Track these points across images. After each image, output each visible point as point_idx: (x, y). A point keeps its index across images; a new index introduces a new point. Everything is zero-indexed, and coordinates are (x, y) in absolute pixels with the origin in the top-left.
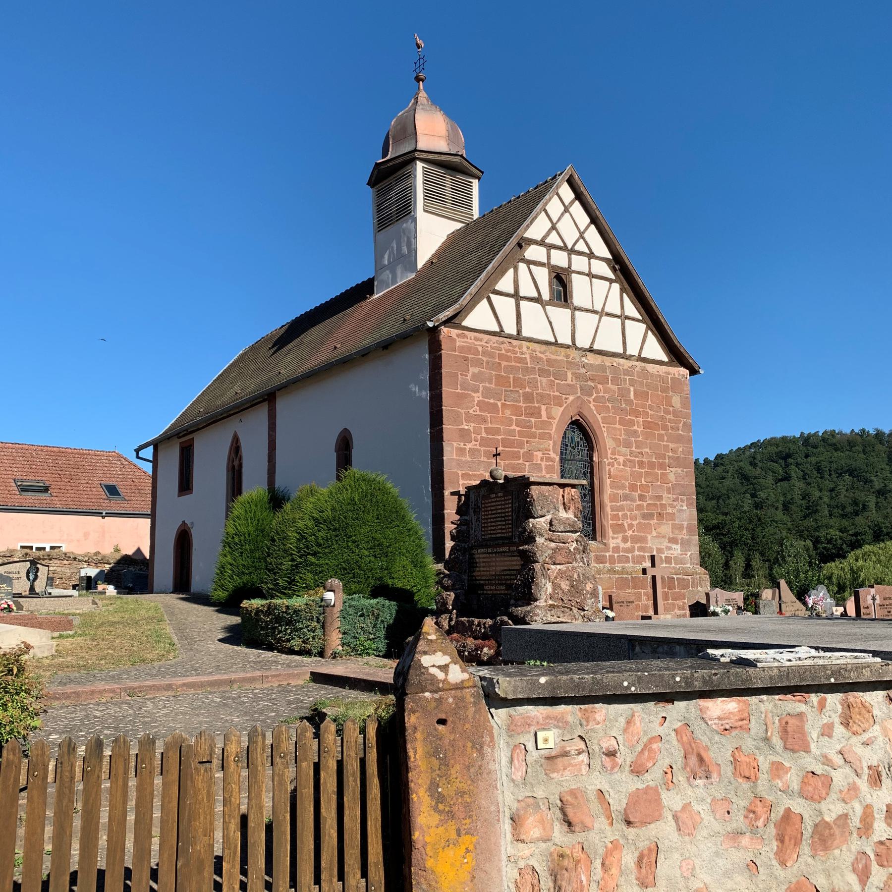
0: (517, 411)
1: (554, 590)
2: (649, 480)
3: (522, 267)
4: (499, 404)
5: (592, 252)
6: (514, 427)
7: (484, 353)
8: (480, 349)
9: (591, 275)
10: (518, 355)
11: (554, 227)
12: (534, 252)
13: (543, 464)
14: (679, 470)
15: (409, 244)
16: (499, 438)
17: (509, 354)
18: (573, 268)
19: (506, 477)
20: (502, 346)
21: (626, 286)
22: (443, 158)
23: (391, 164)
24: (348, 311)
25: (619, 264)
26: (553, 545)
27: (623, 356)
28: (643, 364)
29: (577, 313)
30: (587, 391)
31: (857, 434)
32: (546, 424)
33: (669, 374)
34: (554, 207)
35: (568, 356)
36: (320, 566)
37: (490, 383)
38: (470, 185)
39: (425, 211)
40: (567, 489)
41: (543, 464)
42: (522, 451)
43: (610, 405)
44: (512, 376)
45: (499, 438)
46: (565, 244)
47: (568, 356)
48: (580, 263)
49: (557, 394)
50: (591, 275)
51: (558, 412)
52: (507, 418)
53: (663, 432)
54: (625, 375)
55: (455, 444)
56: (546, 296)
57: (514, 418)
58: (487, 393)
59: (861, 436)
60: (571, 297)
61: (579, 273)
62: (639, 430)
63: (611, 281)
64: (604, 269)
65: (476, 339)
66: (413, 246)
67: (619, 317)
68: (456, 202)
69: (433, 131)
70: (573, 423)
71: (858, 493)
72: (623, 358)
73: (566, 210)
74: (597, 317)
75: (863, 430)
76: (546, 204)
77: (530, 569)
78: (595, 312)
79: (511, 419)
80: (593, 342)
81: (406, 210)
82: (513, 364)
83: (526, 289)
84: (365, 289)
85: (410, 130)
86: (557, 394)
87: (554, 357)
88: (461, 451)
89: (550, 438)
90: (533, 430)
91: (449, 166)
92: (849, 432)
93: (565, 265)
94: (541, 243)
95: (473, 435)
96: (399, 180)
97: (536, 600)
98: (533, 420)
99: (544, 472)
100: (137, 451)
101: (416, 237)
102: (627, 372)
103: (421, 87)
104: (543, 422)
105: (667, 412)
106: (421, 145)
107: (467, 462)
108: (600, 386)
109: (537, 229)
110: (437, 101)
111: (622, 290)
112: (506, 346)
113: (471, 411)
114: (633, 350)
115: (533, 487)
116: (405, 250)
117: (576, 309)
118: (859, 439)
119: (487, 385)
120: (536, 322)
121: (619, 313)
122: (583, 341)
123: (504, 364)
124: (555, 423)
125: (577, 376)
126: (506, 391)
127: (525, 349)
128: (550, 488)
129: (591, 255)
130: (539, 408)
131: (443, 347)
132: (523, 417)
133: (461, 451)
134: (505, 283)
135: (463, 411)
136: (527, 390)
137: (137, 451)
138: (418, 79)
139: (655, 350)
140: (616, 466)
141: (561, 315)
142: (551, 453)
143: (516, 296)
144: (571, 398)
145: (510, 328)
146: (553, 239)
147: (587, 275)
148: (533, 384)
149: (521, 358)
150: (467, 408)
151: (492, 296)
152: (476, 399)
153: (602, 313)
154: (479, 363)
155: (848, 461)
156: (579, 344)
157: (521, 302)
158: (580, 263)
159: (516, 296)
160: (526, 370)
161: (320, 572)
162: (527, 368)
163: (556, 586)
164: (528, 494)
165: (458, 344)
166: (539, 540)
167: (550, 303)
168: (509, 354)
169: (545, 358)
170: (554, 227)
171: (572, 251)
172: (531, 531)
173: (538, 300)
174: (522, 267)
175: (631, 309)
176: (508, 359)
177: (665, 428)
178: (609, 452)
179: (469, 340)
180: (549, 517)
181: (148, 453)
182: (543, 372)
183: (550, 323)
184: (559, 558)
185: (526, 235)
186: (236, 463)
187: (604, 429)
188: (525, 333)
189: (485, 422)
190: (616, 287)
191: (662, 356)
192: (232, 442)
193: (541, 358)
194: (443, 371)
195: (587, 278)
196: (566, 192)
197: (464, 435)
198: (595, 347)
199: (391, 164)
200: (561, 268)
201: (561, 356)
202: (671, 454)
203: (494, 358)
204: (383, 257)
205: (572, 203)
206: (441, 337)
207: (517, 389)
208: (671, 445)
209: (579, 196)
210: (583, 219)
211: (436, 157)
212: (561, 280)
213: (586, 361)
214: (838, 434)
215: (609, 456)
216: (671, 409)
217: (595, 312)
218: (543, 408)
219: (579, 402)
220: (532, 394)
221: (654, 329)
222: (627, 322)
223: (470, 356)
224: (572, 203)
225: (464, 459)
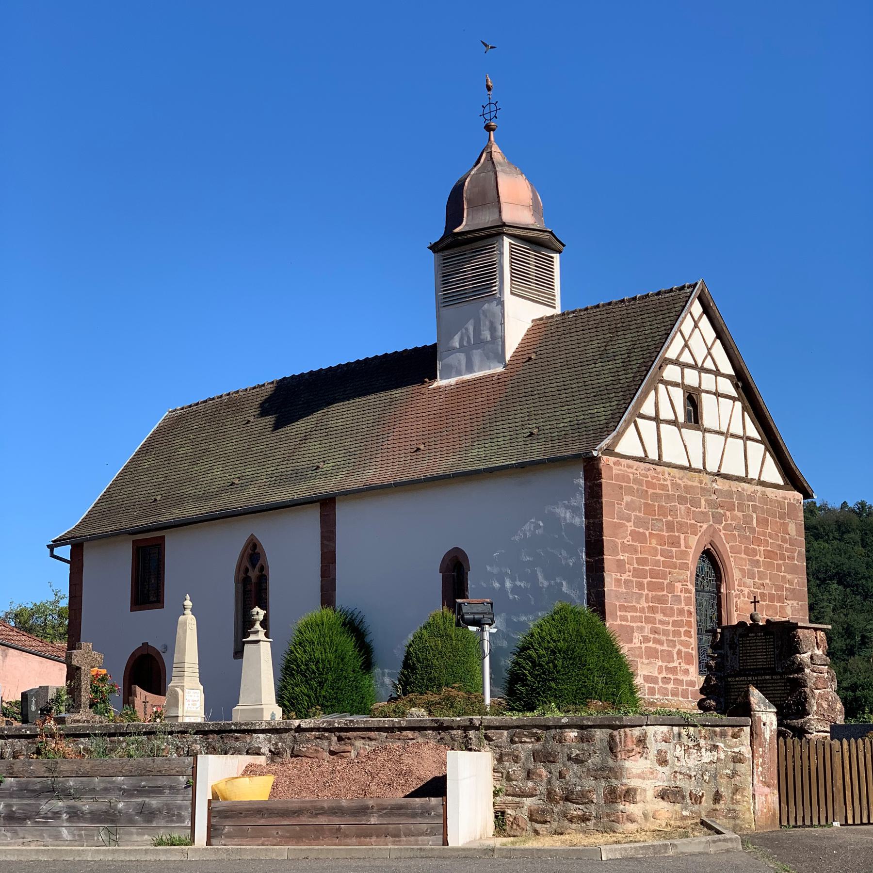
0: (661, 541)
1: (818, 708)
2: (770, 613)
3: (661, 387)
4: (647, 533)
5: (718, 370)
6: (659, 557)
7: (636, 481)
8: (631, 476)
9: (717, 394)
10: (662, 482)
11: (686, 345)
12: (671, 373)
13: (683, 595)
14: (795, 603)
15: (493, 329)
16: (648, 568)
17: (654, 481)
18: (703, 387)
19: (768, 621)
20: (648, 473)
21: (747, 404)
22: (532, 234)
23: (472, 235)
24: (397, 393)
25: (742, 381)
26: (815, 674)
27: (745, 480)
28: (764, 489)
29: (707, 434)
30: (718, 518)
31: (852, 510)
32: (684, 554)
33: (785, 498)
34: (687, 325)
35: (701, 482)
36: (561, 691)
37: (640, 512)
38: (551, 260)
39: (512, 293)
40: (819, 632)
41: (683, 595)
42: (666, 582)
43: (737, 534)
44: (656, 504)
45: (648, 568)
46: (696, 364)
47: (701, 482)
48: (708, 382)
49: (693, 522)
50: (717, 394)
51: (693, 540)
52: (654, 548)
53: (781, 562)
54: (748, 501)
55: (614, 576)
56: (681, 419)
57: (659, 547)
58: (639, 522)
59: (859, 515)
60: (702, 418)
61: (708, 392)
62: (761, 559)
63: (733, 399)
64: (727, 387)
65: (629, 467)
66: (499, 334)
67: (741, 438)
68: (539, 281)
69: (517, 200)
70: (704, 552)
71: (852, 616)
72: (745, 482)
73: (696, 326)
74: (723, 438)
75: (862, 505)
76: (681, 324)
77: (801, 693)
78: (721, 433)
79: (657, 550)
80: (720, 467)
81: (485, 288)
82: (658, 491)
83: (666, 413)
84: (417, 365)
85: (492, 194)
86: (693, 522)
87: (690, 483)
88: (618, 581)
89: (688, 568)
90: (674, 560)
91: (537, 242)
92: (838, 505)
93: (696, 384)
94: (676, 362)
95: (627, 566)
96: (477, 251)
97: (809, 714)
98: (674, 549)
99: (683, 604)
100: (51, 548)
101: (502, 324)
102: (750, 498)
103: (492, 139)
104: (682, 551)
105: (784, 540)
106: (509, 215)
107: (622, 593)
108: (728, 513)
109: (673, 350)
110: (521, 163)
111: (744, 409)
112: (652, 473)
113: (625, 541)
114: (753, 474)
115: (799, 630)
116: (486, 335)
117: (706, 431)
118: (855, 519)
119: (638, 514)
120: (678, 446)
121: (741, 434)
122: (712, 467)
123: (650, 491)
124: (691, 551)
125: (709, 503)
126: (653, 520)
127: (666, 476)
128: (809, 631)
129: (717, 373)
130: (679, 537)
131: (603, 476)
132: (666, 547)
133: (618, 581)
134: (648, 408)
135: (619, 541)
136: (670, 518)
137: (51, 548)
138: (489, 128)
139: (772, 474)
140: (742, 598)
141: (693, 436)
142: (688, 584)
143: (656, 419)
144: (705, 526)
145: (653, 455)
146: (686, 358)
147: (715, 394)
148: (673, 511)
149: (663, 485)
150: (622, 538)
151: (639, 420)
152: (629, 529)
153: (727, 435)
154: (630, 491)
155: (838, 559)
156: (709, 469)
157: (661, 425)
158: (708, 382)
159: (656, 419)
160: (669, 498)
161: (560, 697)
162: (668, 495)
163: (819, 705)
164: (795, 636)
165: (614, 472)
166: (807, 671)
167: (684, 426)
168: (654, 481)
169: (683, 484)
170: (686, 345)
171: (702, 370)
172: (800, 664)
173: (674, 423)
174: (661, 387)
175: (752, 431)
176: (653, 486)
177: (782, 558)
178: (736, 583)
179: (622, 468)
180: (809, 653)
181: (65, 551)
182: (682, 500)
183: (685, 446)
184: (820, 685)
185: (667, 356)
186: (253, 574)
187: (732, 559)
188: (665, 459)
189: (636, 551)
190: (738, 404)
191: (779, 480)
192: (246, 547)
193: (680, 485)
194: (604, 500)
195: (714, 397)
196: (696, 308)
197: (620, 566)
198: (722, 471)
199: (472, 235)
200: (693, 388)
201: (694, 481)
202: (787, 586)
203: (642, 486)
204: (451, 337)
205: (700, 317)
206: (601, 465)
207: (661, 517)
208: (789, 576)
209: (707, 310)
210: (710, 334)
211: (525, 233)
212: (692, 400)
213: (716, 487)
214: (820, 509)
215: (736, 587)
216: (787, 536)
217: (721, 433)
218: (682, 536)
219: (712, 530)
220: (673, 522)
221: (771, 450)
222: (749, 443)
223: (624, 484)
224: (700, 317)
225: (620, 590)
